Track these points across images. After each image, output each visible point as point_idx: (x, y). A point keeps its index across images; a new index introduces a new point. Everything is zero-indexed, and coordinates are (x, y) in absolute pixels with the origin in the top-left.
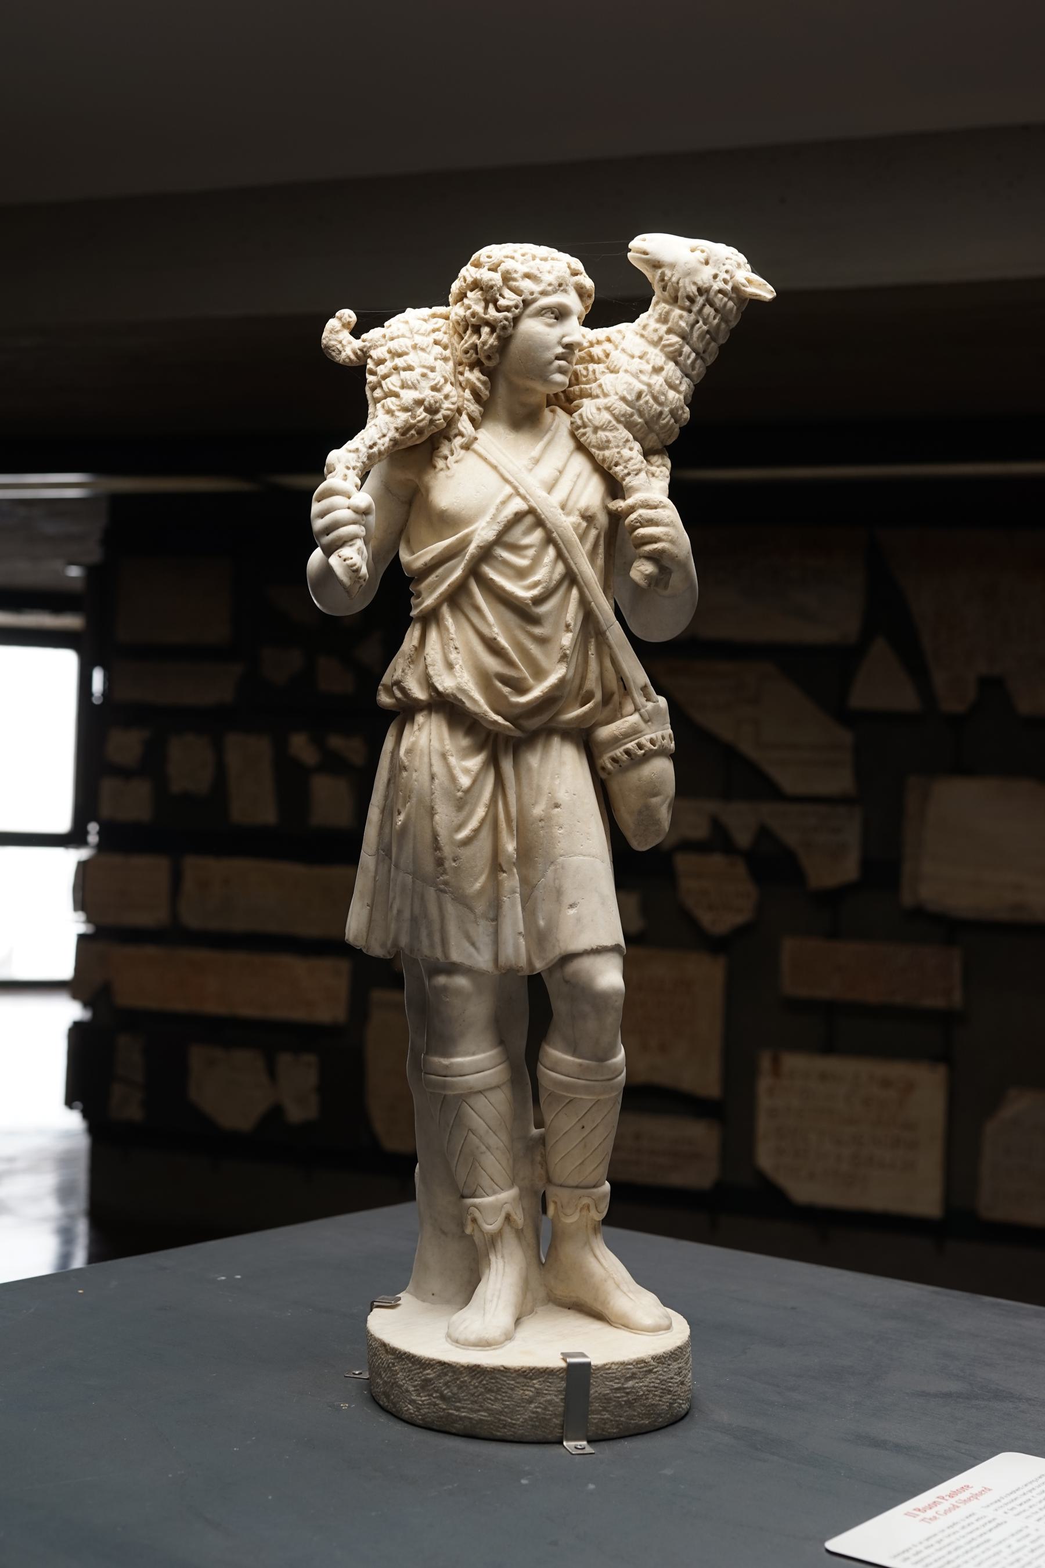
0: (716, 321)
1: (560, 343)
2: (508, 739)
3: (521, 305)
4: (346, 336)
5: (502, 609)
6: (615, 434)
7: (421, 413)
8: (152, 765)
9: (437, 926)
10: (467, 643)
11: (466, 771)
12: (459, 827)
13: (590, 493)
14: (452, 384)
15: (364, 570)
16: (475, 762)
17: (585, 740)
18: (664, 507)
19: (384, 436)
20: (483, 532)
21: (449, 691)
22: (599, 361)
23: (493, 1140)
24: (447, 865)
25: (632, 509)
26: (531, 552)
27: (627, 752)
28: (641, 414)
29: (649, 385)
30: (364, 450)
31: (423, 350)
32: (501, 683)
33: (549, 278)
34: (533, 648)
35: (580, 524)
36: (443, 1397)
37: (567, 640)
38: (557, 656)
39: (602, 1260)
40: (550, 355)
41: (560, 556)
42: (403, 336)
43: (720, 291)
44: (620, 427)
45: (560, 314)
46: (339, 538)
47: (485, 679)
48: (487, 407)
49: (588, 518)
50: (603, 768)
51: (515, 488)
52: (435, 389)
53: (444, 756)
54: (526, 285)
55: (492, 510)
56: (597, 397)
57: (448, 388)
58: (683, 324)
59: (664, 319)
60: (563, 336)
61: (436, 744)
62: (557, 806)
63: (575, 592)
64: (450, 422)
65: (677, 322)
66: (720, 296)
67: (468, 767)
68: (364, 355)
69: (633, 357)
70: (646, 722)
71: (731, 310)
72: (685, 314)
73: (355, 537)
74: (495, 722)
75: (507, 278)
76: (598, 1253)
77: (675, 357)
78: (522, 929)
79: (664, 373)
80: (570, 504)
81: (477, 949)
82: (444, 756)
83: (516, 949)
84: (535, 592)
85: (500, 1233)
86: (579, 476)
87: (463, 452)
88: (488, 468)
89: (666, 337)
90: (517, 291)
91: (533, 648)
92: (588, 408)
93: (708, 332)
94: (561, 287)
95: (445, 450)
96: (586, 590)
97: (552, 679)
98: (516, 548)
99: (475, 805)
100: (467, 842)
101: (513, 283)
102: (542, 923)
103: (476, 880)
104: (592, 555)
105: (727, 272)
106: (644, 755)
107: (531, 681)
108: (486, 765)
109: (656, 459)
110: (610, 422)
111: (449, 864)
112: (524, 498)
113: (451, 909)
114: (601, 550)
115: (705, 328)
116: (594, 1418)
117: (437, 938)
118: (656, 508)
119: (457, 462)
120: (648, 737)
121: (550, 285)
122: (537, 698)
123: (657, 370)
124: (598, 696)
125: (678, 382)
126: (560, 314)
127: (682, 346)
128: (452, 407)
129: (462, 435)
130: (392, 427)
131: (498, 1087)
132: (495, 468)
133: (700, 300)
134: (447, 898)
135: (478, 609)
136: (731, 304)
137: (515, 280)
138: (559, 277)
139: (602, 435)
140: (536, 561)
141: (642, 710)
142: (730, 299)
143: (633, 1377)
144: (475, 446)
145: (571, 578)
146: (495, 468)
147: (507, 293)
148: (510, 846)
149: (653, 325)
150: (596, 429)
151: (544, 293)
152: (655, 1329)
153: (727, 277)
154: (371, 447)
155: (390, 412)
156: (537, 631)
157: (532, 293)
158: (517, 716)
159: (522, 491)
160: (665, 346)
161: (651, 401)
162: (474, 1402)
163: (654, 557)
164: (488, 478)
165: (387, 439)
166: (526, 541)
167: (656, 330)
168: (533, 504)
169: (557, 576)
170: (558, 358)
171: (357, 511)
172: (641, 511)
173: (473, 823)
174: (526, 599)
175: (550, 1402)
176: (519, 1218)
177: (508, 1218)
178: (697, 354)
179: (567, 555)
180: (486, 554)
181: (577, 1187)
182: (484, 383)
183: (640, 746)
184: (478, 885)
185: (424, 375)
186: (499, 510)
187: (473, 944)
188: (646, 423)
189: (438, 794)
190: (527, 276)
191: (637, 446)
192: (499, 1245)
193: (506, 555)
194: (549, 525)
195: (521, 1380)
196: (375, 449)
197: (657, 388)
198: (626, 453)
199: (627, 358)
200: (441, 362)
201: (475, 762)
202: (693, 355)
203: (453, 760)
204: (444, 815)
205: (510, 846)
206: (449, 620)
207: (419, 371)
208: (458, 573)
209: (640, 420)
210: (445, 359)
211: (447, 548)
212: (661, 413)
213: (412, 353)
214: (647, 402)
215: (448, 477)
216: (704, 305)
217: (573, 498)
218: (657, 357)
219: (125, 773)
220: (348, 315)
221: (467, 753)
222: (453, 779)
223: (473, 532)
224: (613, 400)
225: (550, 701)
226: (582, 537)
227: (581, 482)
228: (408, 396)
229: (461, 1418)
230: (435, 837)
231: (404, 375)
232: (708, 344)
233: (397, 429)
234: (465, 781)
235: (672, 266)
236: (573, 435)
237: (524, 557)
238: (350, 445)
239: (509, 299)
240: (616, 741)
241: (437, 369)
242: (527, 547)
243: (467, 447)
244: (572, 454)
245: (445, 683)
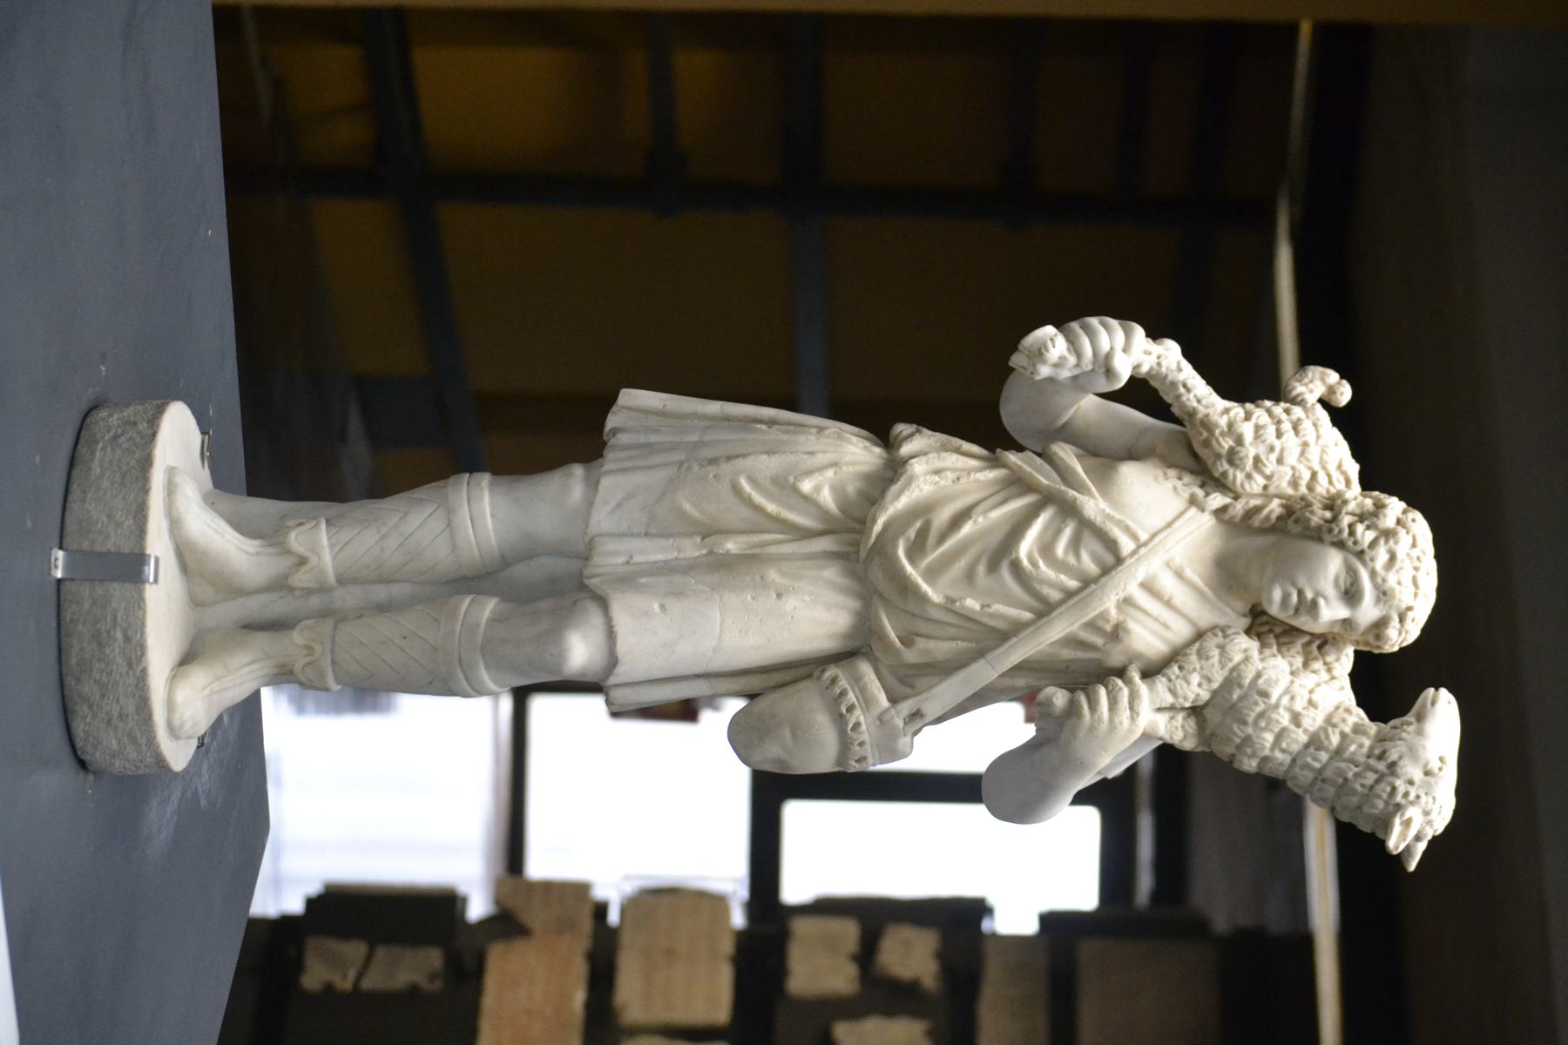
0: (1358, 787)
1: (1318, 594)
2: (856, 544)
3: (1359, 548)
4: (1319, 390)
5: (1005, 529)
6: (1217, 666)
7: (1227, 443)
8: (882, 994)
9: (641, 463)
10: (964, 493)
11: (818, 489)
12: (753, 481)
13: (1147, 639)
14: (1265, 487)
15: (1044, 371)
16: (827, 498)
17: (856, 648)
18: (1133, 719)
19: (1199, 401)
20: (1093, 505)
21: (908, 467)
22: (1306, 665)
23: (392, 543)
24: (710, 468)
25: (1129, 682)
26: (1072, 560)
27: (843, 694)
28: (1242, 698)
29: (1277, 706)
30: (1181, 377)
31: (1302, 453)
32: (923, 529)
33: (1391, 579)
34: (961, 565)
35: (1108, 621)
36: (116, 437)
37: (972, 604)
38: (951, 593)
39: (247, 669)
40: (1302, 581)
41: (1069, 594)
42: (1318, 437)
43: (1394, 789)
44: (1225, 672)
45: (1351, 595)
46: (1077, 336)
47: (923, 510)
48: (1238, 525)
49: (1117, 634)
50: (823, 671)
51: (1145, 544)
52: (1257, 460)
53: (835, 464)
54: (1382, 556)
55: (1118, 516)
56: (1261, 652)
57: (1261, 481)
58: (1353, 748)
59: (1358, 730)
60: (1325, 598)
61: (848, 458)
62: (779, 596)
63: (1028, 615)
64: (1221, 484)
65: (1353, 742)
66: (1389, 789)
67: (822, 488)
68: (1296, 401)
69: (1311, 692)
70: (880, 718)
71: (1374, 806)
72: (1365, 750)
73: (1078, 354)
74: (874, 521)
75: (1388, 534)
76: (256, 666)
77: (1315, 742)
78: (636, 559)
79: (1293, 727)
80: (1132, 611)
81: (613, 511)
82: (835, 464)
83: (611, 557)
84: (1025, 562)
85: (288, 552)
86: (1165, 625)
87: (1186, 495)
88: (1169, 518)
89: (1337, 731)
90: (1373, 544)
91: (961, 565)
92: (1243, 645)
93: (1346, 780)
94: (1383, 594)
95: (1187, 478)
96: (1032, 629)
97: (925, 587)
98: (1075, 544)
99: (779, 502)
100: (737, 490)
101: (1382, 541)
102: (643, 580)
103: (693, 504)
104: (1073, 641)
105: (1418, 797)
106: (841, 715)
107: (924, 563)
108: (823, 512)
109: (1191, 724)
110: (1230, 660)
111: (711, 471)
112: (1134, 553)
113: (660, 476)
114: (1081, 654)
115: (1350, 775)
116: (85, 590)
117: (628, 464)
118: (1131, 708)
119: (1175, 488)
120: (862, 719)
121: (1384, 580)
122: (903, 568)
123: (1296, 719)
124: (910, 656)
125: (1284, 745)
126: (1351, 595)
127: (1326, 750)
128: (1238, 482)
129: (1207, 494)
130: (1211, 411)
131: (454, 548)
132: (1169, 525)
133: (1381, 766)
134: (672, 471)
135: (1004, 502)
136: (1380, 804)
137: (1387, 542)
138: (1393, 590)
139: (1216, 653)
140: (1061, 566)
141: (893, 711)
142: (1387, 803)
143: (127, 639)
144: (1193, 510)
145: (1045, 610)
146: (1169, 525)
147: (1370, 535)
148: (731, 546)
149: (1352, 720)
150: (1222, 648)
151: (1373, 574)
152: (170, 705)
153: (1412, 797)
154: (1185, 386)
155: (1227, 411)
156: (981, 569)
157: (1372, 560)
158: (883, 549)
159: (1143, 551)
160: (1326, 730)
161: (1259, 709)
162: (111, 462)
163: (1072, 710)
164: (1161, 529)
165: (1195, 404)
166: (1085, 556)
167: (1344, 721)
168: (1129, 562)
169: (1046, 591)
170: (1300, 593)
171: (1109, 356)
172: (1126, 691)
173: (758, 498)
174: (1017, 552)
175: (107, 537)
176: (301, 579)
177: (302, 561)
178: (1320, 771)
179: (1071, 602)
180: (1069, 510)
181: (333, 642)
182: (1268, 518)
183: (850, 709)
184: (687, 506)
185: (1272, 449)
186: (1119, 523)
187: (619, 505)
188: (1233, 706)
189: (791, 458)
190: (1393, 557)
191: (1205, 695)
192: (271, 550)
193: (1068, 532)
194: (1103, 580)
195: (134, 507)
196: (1182, 390)
197: (1274, 716)
198: (1195, 679)
199: (1310, 686)
200: (1288, 477)
201: (827, 498)
202: (1317, 765)
203: (830, 473)
204: (767, 465)
205: (731, 546)
206: (992, 475)
207: (1277, 444)
208: (1045, 482)
209: (1235, 697)
210: (1294, 483)
211: (1073, 471)
212: (1245, 723)
213: (1299, 442)
214: (1256, 704)
215: (1156, 478)
216: (1376, 772)
217: (1138, 615)
218: (1314, 720)
219: (866, 955)
220: (1345, 394)
221: (838, 490)
222: (809, 473)
223: (1093, 496)
224: (1256, 664)
225: (906, 588)
226: (1092, 625)
227: (1160, 629)
228: (1247, 430)
229: (93, 453)
230: (744, 456)
231: (1271, 429)
232: (1333, 783)
233: (1207, 415)
234: (806, 486)
235: (1420, 733)
236: (1213, 629)
237: (1066, 552)
238: (1187, 367)
239: (1365, 536)
240: (857, 680)
241: (1281, 468)
242: (1078, 556)
243: (1193, 501)
244: (1192, 622)
245: (918, 467)
